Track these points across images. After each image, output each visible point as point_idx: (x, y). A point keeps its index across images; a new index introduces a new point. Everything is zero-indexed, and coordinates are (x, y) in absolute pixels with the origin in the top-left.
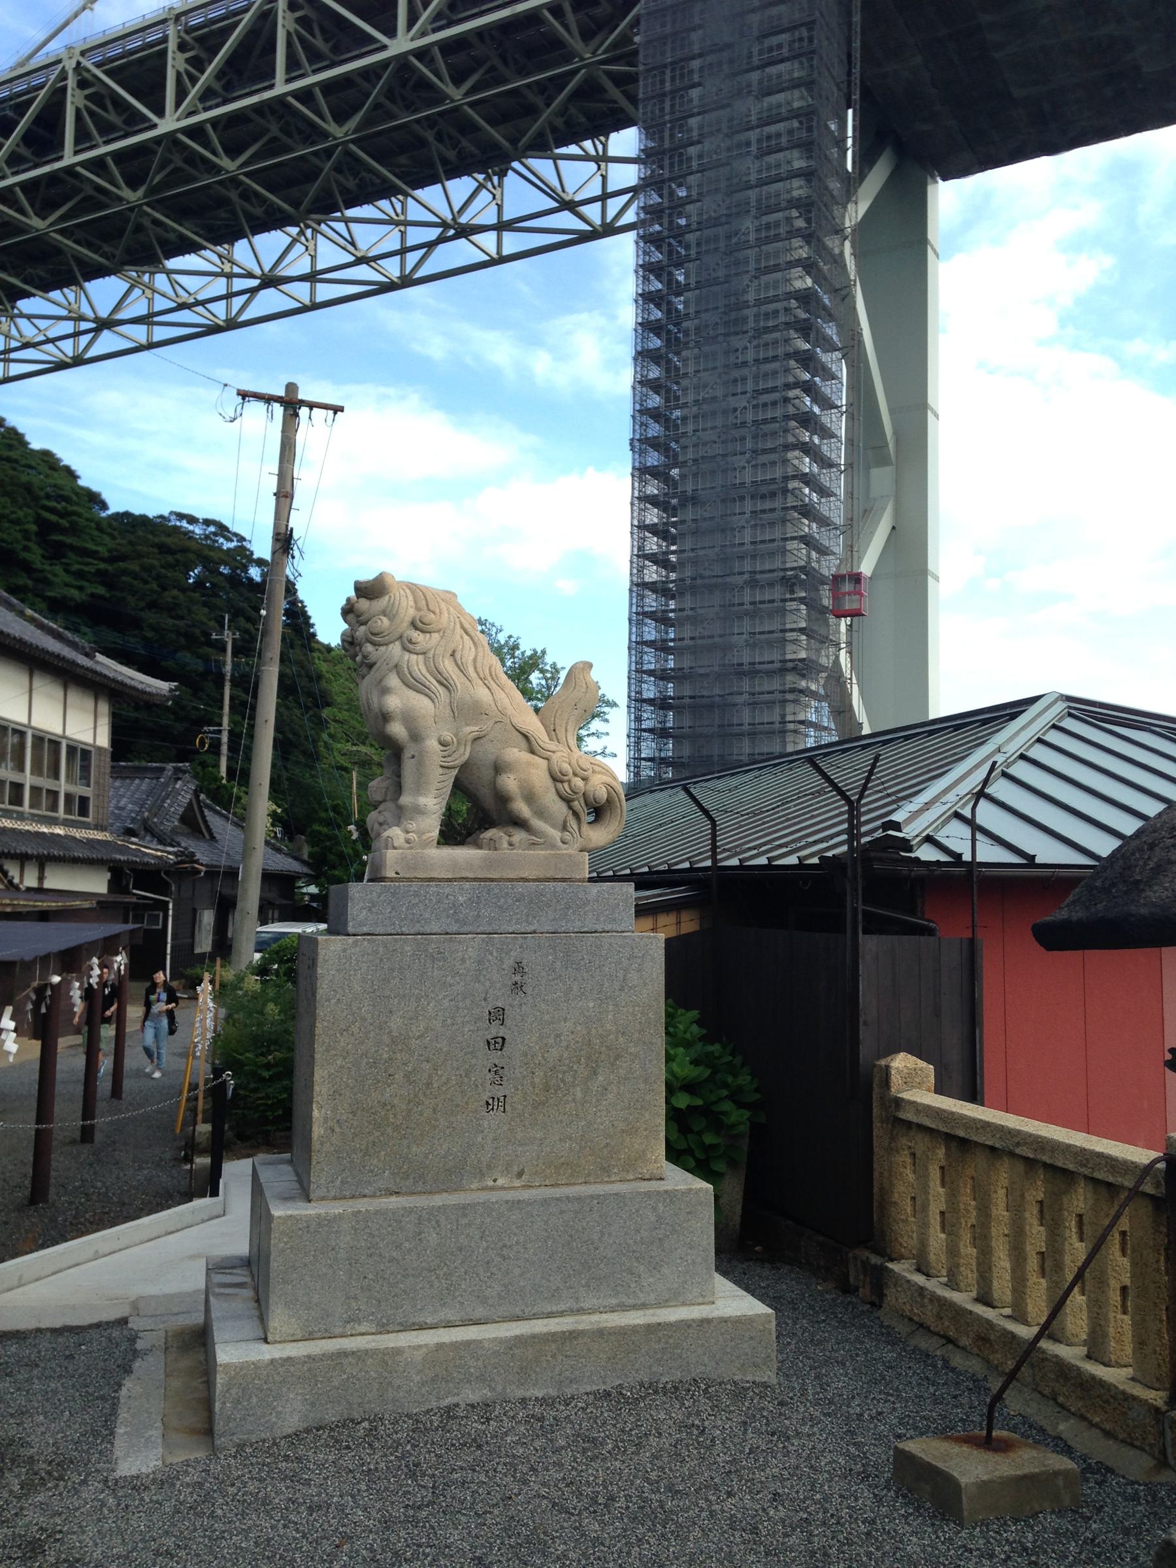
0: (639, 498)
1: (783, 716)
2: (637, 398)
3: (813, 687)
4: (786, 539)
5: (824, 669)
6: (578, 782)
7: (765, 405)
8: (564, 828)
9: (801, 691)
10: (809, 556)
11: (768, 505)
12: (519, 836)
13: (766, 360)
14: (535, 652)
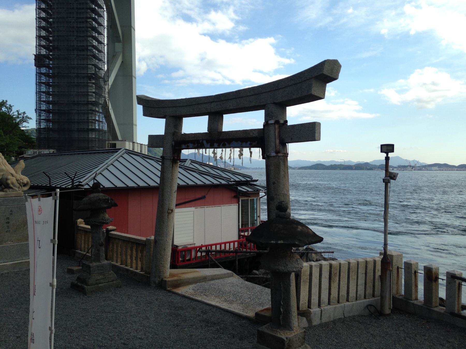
0: (39, 45)
1: (88, 117)
2: (37, 13)
3: (97, 109)
4: (88, 64)
5: (101, 104)
6: (21, 181)
7: (80, 22)
8: (19, 188)
9: (93, 111)
10: (95, 70)
11: (82, 53)
12: (11, 190)
13: (80, 9)
14: (3, 101)
